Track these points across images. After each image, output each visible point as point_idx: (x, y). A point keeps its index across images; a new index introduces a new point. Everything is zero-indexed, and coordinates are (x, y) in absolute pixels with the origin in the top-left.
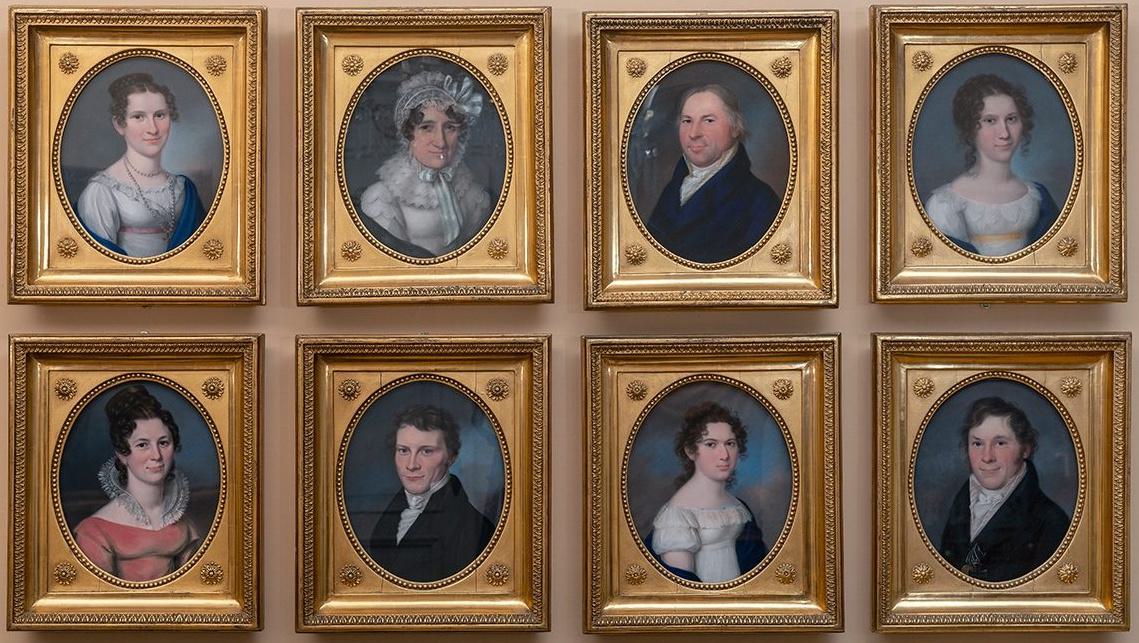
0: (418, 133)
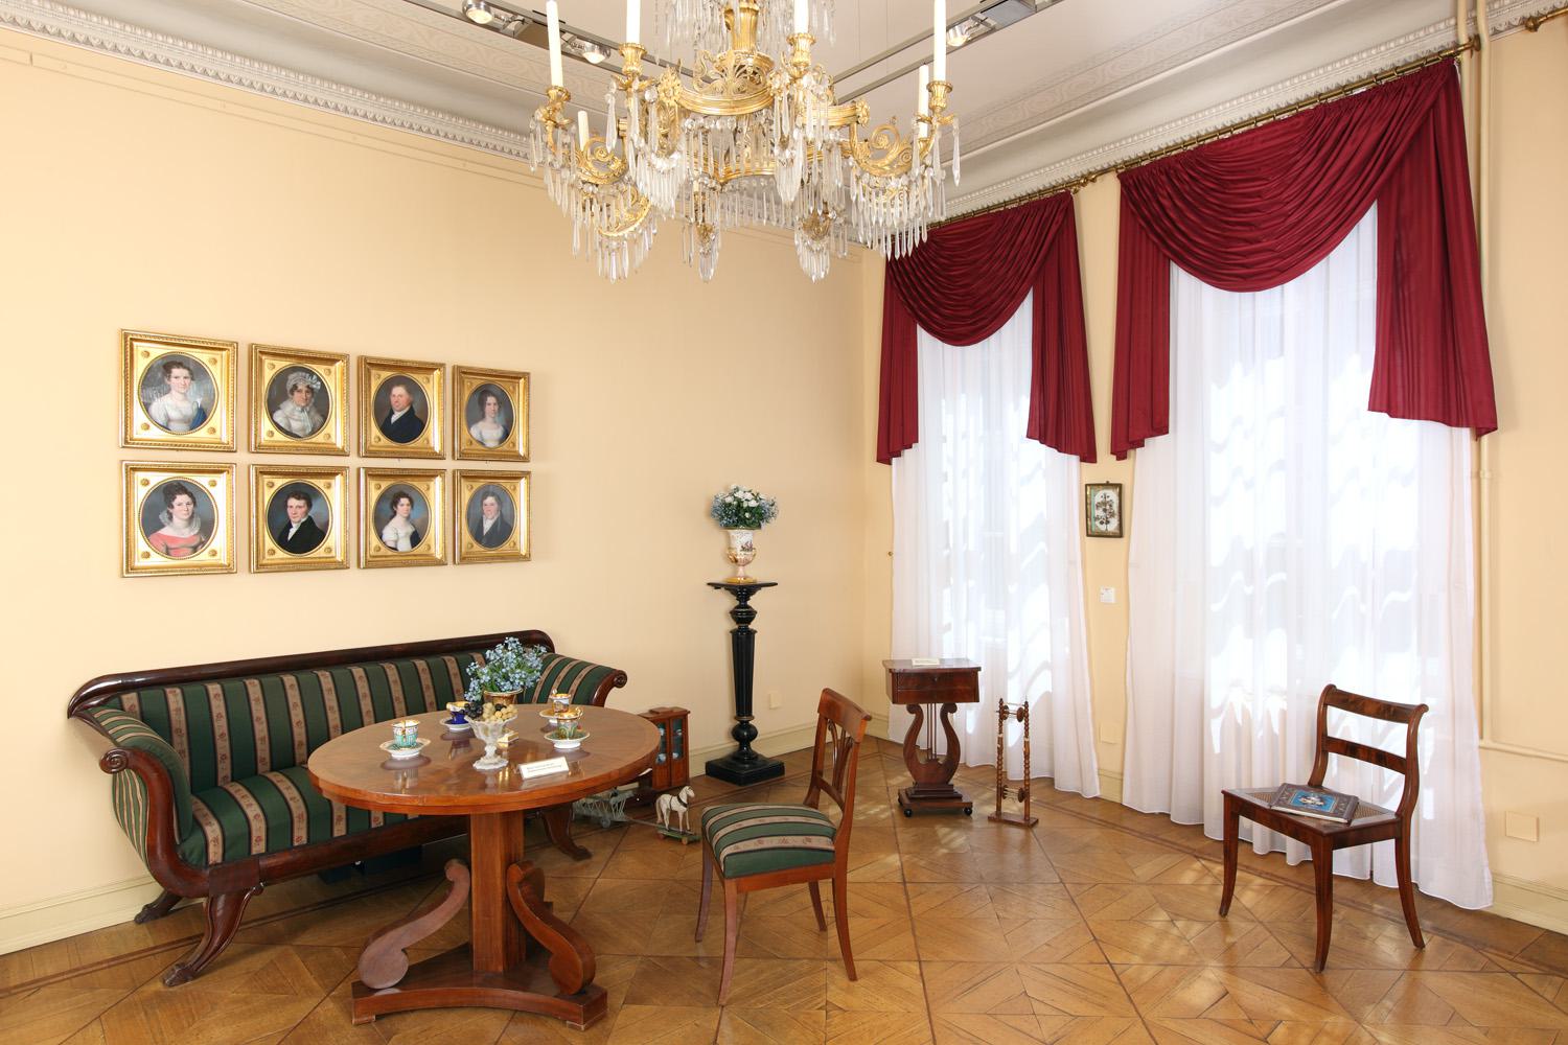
0: (296, 393)
